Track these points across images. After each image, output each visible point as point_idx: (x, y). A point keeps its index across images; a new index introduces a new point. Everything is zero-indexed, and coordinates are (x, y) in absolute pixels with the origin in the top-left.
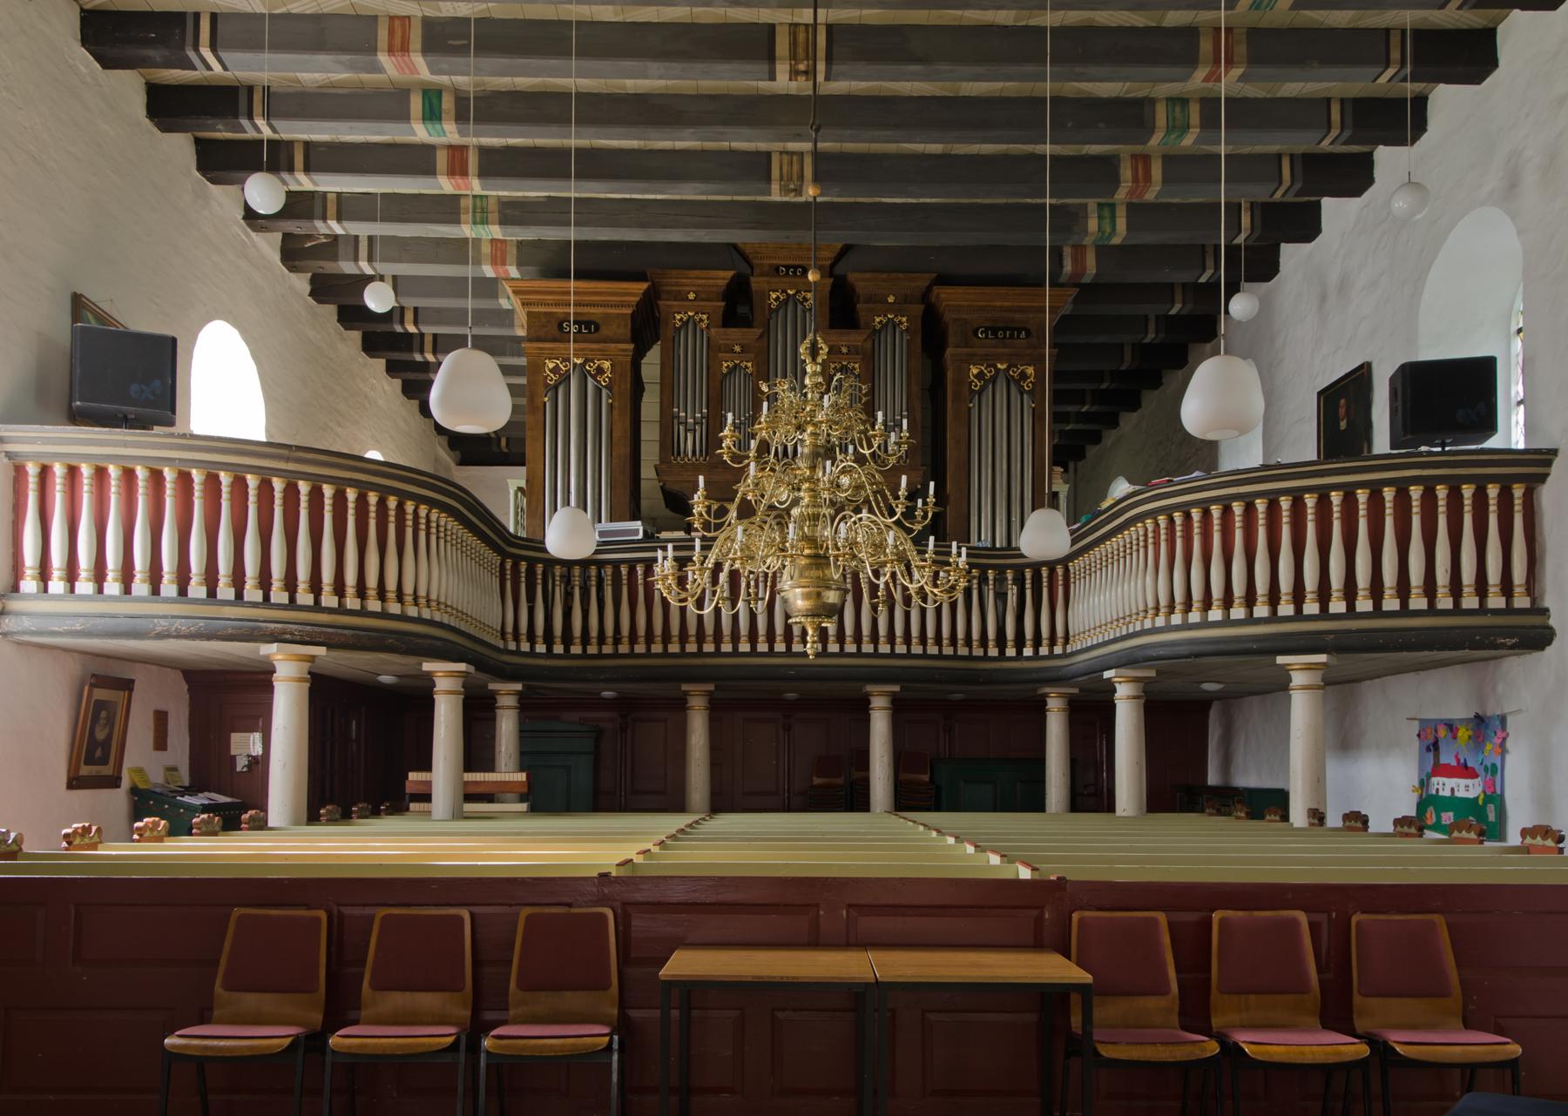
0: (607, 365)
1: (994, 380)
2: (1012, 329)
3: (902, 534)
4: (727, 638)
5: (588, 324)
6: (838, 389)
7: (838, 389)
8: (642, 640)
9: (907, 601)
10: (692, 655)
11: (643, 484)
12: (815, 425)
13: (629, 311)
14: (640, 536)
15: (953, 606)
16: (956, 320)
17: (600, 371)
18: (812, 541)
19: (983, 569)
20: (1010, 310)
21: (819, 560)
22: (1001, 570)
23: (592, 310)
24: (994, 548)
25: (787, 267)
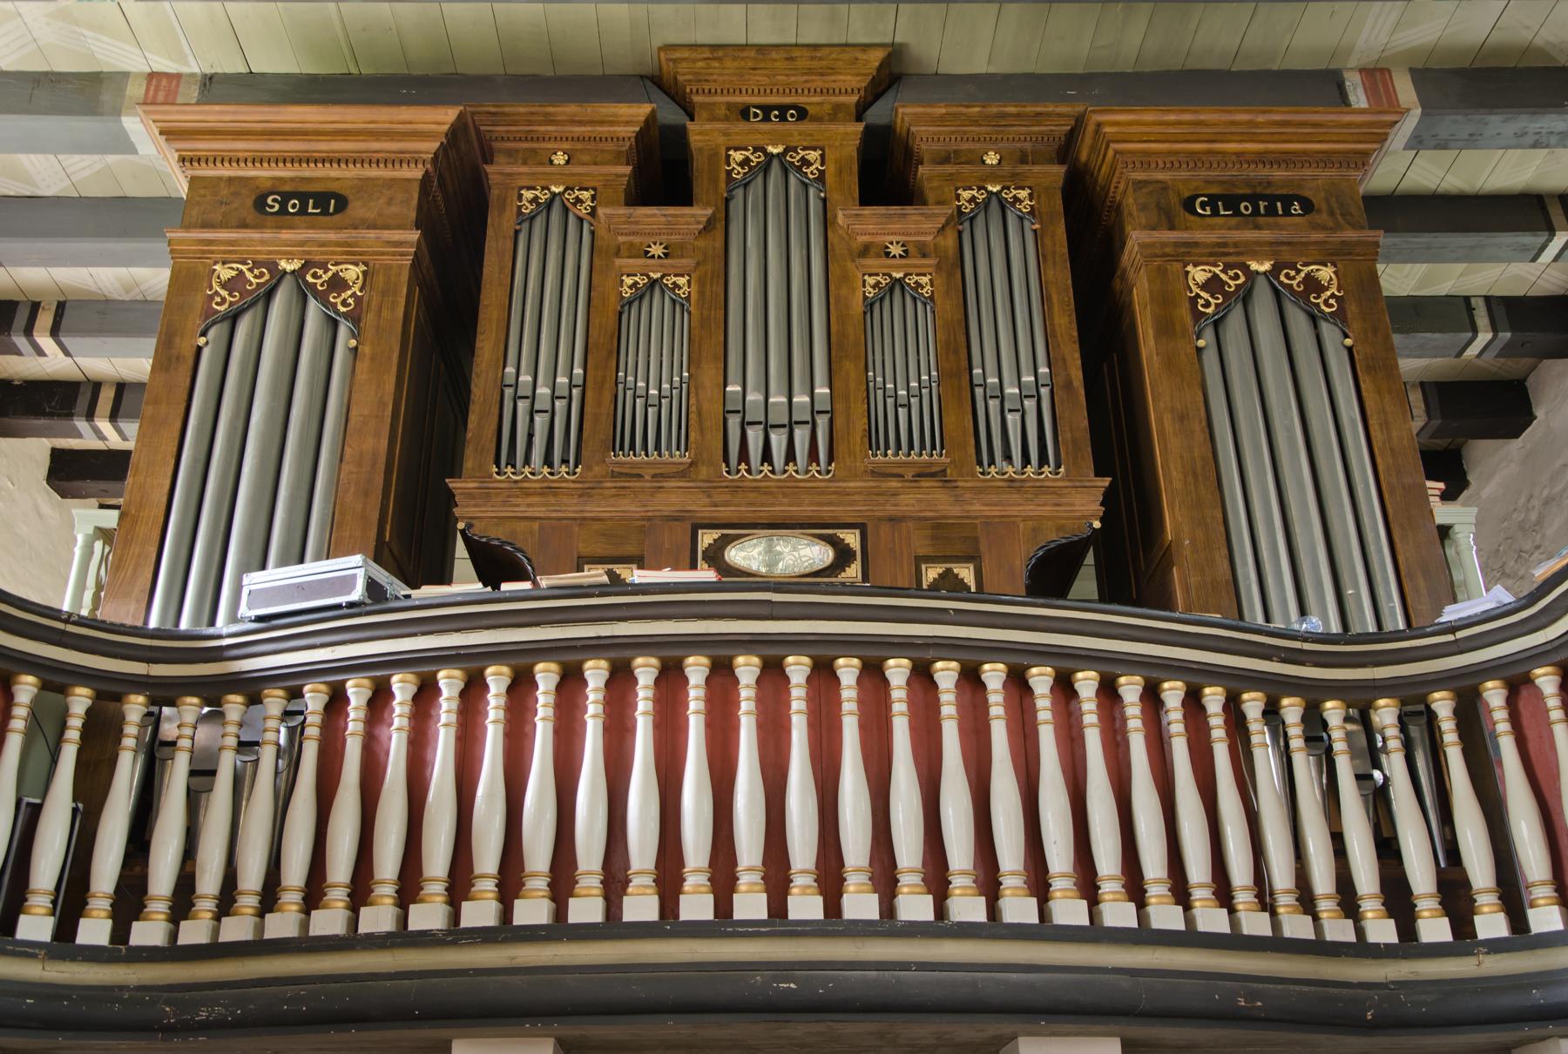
1: (1245, 296)
2: (1271, 200)
5: (322, 199)
13: (417, 173)
14: (357, 594)
16: (1139, 185)
20: (1261, 159)
23: (333, 172)
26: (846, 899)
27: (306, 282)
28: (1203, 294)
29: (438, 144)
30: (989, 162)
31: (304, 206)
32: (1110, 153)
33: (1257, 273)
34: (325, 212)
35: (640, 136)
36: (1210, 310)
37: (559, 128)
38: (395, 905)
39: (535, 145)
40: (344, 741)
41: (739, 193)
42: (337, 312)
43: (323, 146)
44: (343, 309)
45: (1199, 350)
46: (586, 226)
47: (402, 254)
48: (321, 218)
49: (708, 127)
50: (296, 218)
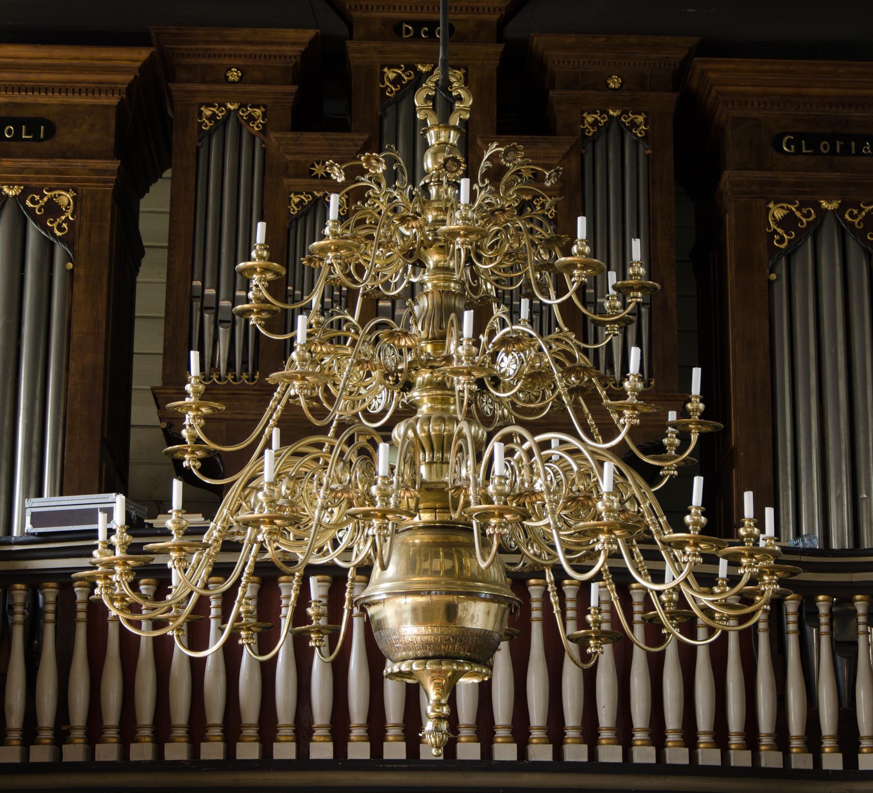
0: (65, 198)
1: (815, 230)
3: (635, 484)
4: (286, 732)
5: (33, 124)
6: (496, 174)
7: (496, 174)
8: (112, 734)
9: (655, 633)
10: (213, 765)
11: (135, 436)
12: (444, 249)
13: (113, 100)
15: (748, 640)
17: (53, 210)
18: (438, 495)
19: (808, 595)
21: (451, 536)
22: (843, 595)
23: (42, 99)
24: (826, 549)
25: (418, 25)
26: (459, 746)
27: (26, 207)
28: (779, 230)
29: (132, 77)
30: (612, 85)
31: (18, 132)
32: (714, 93)
33: (826, 210)
34: (37, 139)
35: (305, 55)
36: (783, 246)
37: (234, 47)
38: (153, 742)
39: (212, 61)
40: (107, 624)
41: (390, 110)
42: (54, 235)
43: (32, 77)
44: (59, 234)
45: (770, 283)
46: (258, 140)
47: (105, 182)
48: (33, 143)
49: (365, 45)
50: (12, 143)
